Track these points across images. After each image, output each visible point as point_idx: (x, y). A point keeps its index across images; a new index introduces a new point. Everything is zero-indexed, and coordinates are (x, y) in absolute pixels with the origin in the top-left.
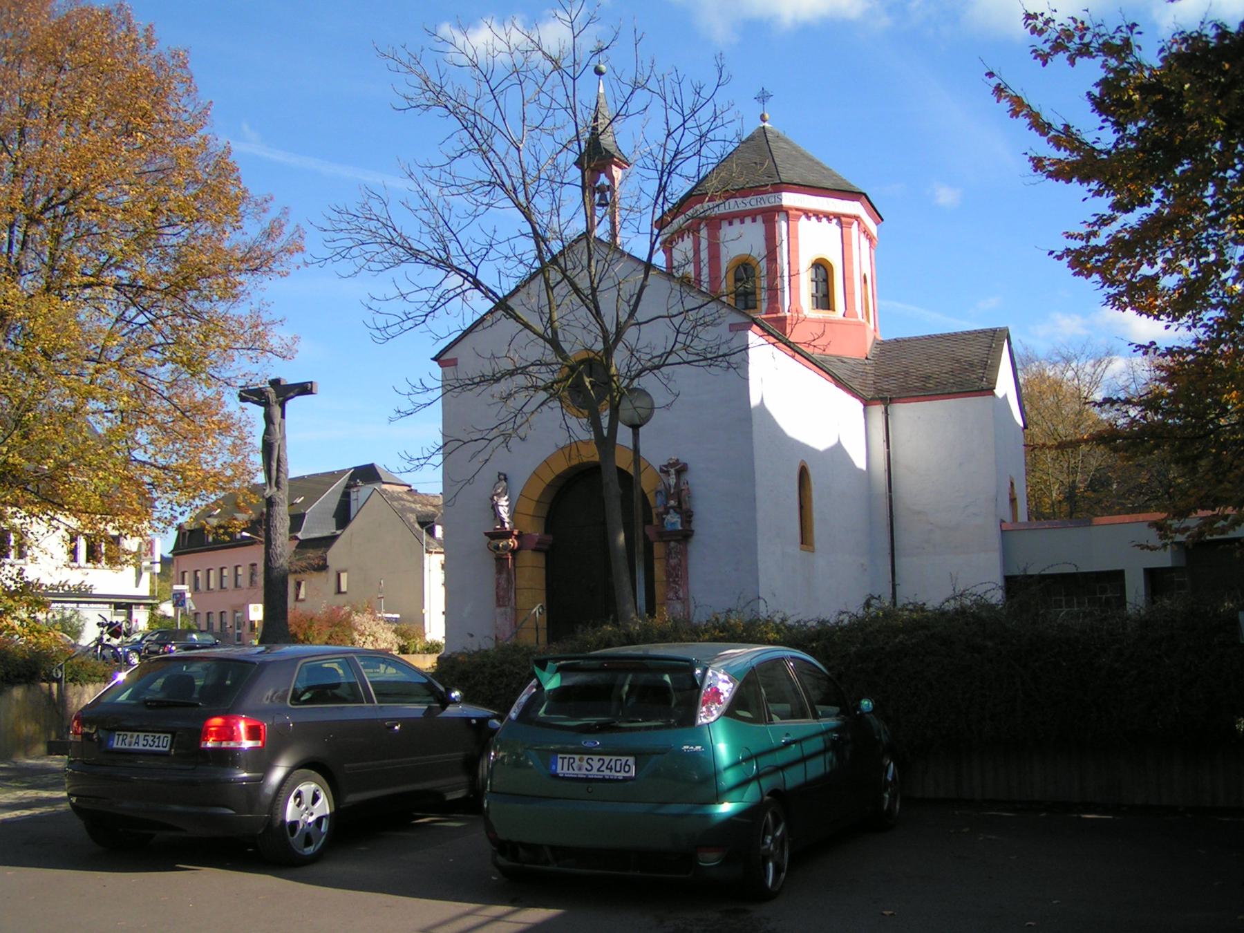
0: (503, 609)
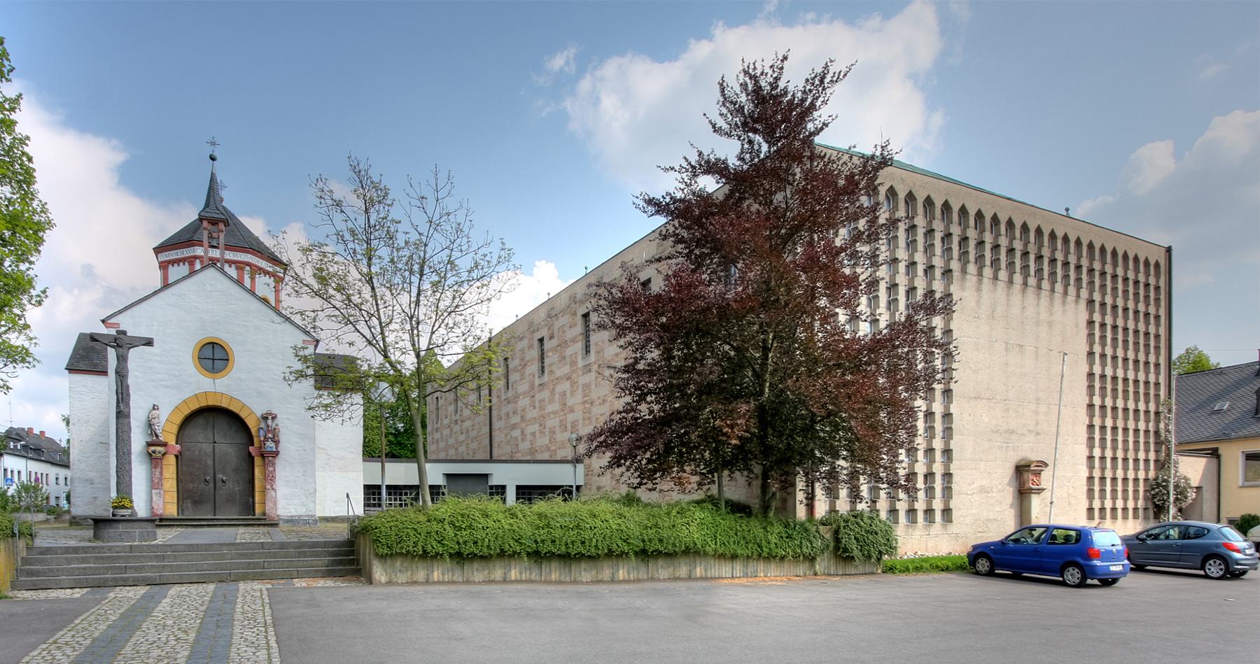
0: (158, 491)
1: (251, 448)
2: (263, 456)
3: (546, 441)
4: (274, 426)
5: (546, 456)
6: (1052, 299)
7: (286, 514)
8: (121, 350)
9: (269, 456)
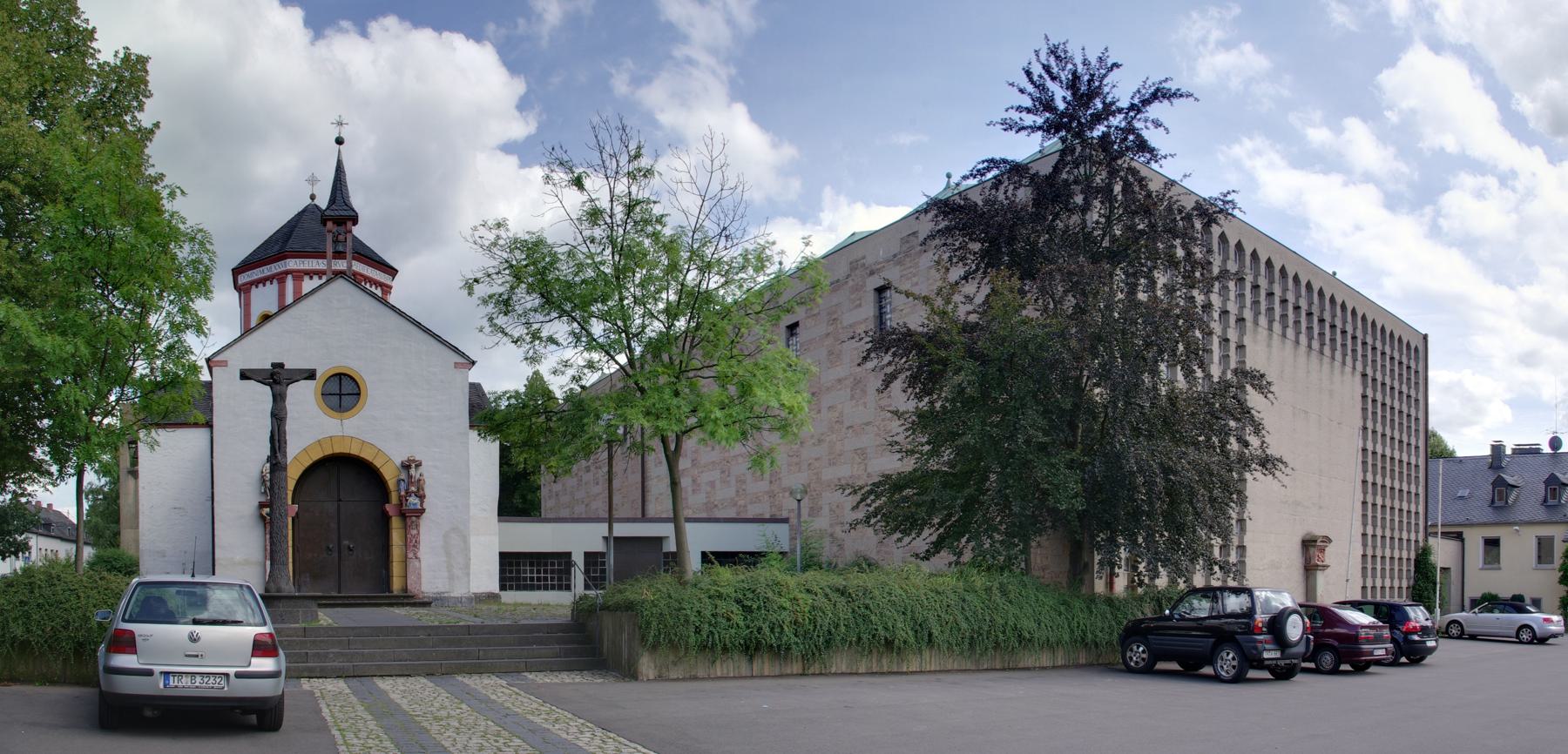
1: (388, 507)
2: (403, 515)
3: (731, 492)
4: (418, 476)
5: (732, 514)
6: (1332, 367)
7: (432, 590)
8: (278, 387)
9: (410, 516)
